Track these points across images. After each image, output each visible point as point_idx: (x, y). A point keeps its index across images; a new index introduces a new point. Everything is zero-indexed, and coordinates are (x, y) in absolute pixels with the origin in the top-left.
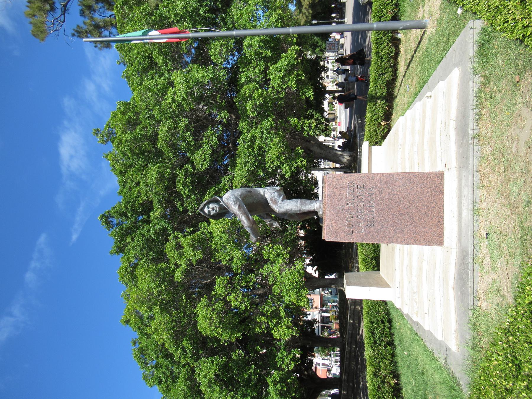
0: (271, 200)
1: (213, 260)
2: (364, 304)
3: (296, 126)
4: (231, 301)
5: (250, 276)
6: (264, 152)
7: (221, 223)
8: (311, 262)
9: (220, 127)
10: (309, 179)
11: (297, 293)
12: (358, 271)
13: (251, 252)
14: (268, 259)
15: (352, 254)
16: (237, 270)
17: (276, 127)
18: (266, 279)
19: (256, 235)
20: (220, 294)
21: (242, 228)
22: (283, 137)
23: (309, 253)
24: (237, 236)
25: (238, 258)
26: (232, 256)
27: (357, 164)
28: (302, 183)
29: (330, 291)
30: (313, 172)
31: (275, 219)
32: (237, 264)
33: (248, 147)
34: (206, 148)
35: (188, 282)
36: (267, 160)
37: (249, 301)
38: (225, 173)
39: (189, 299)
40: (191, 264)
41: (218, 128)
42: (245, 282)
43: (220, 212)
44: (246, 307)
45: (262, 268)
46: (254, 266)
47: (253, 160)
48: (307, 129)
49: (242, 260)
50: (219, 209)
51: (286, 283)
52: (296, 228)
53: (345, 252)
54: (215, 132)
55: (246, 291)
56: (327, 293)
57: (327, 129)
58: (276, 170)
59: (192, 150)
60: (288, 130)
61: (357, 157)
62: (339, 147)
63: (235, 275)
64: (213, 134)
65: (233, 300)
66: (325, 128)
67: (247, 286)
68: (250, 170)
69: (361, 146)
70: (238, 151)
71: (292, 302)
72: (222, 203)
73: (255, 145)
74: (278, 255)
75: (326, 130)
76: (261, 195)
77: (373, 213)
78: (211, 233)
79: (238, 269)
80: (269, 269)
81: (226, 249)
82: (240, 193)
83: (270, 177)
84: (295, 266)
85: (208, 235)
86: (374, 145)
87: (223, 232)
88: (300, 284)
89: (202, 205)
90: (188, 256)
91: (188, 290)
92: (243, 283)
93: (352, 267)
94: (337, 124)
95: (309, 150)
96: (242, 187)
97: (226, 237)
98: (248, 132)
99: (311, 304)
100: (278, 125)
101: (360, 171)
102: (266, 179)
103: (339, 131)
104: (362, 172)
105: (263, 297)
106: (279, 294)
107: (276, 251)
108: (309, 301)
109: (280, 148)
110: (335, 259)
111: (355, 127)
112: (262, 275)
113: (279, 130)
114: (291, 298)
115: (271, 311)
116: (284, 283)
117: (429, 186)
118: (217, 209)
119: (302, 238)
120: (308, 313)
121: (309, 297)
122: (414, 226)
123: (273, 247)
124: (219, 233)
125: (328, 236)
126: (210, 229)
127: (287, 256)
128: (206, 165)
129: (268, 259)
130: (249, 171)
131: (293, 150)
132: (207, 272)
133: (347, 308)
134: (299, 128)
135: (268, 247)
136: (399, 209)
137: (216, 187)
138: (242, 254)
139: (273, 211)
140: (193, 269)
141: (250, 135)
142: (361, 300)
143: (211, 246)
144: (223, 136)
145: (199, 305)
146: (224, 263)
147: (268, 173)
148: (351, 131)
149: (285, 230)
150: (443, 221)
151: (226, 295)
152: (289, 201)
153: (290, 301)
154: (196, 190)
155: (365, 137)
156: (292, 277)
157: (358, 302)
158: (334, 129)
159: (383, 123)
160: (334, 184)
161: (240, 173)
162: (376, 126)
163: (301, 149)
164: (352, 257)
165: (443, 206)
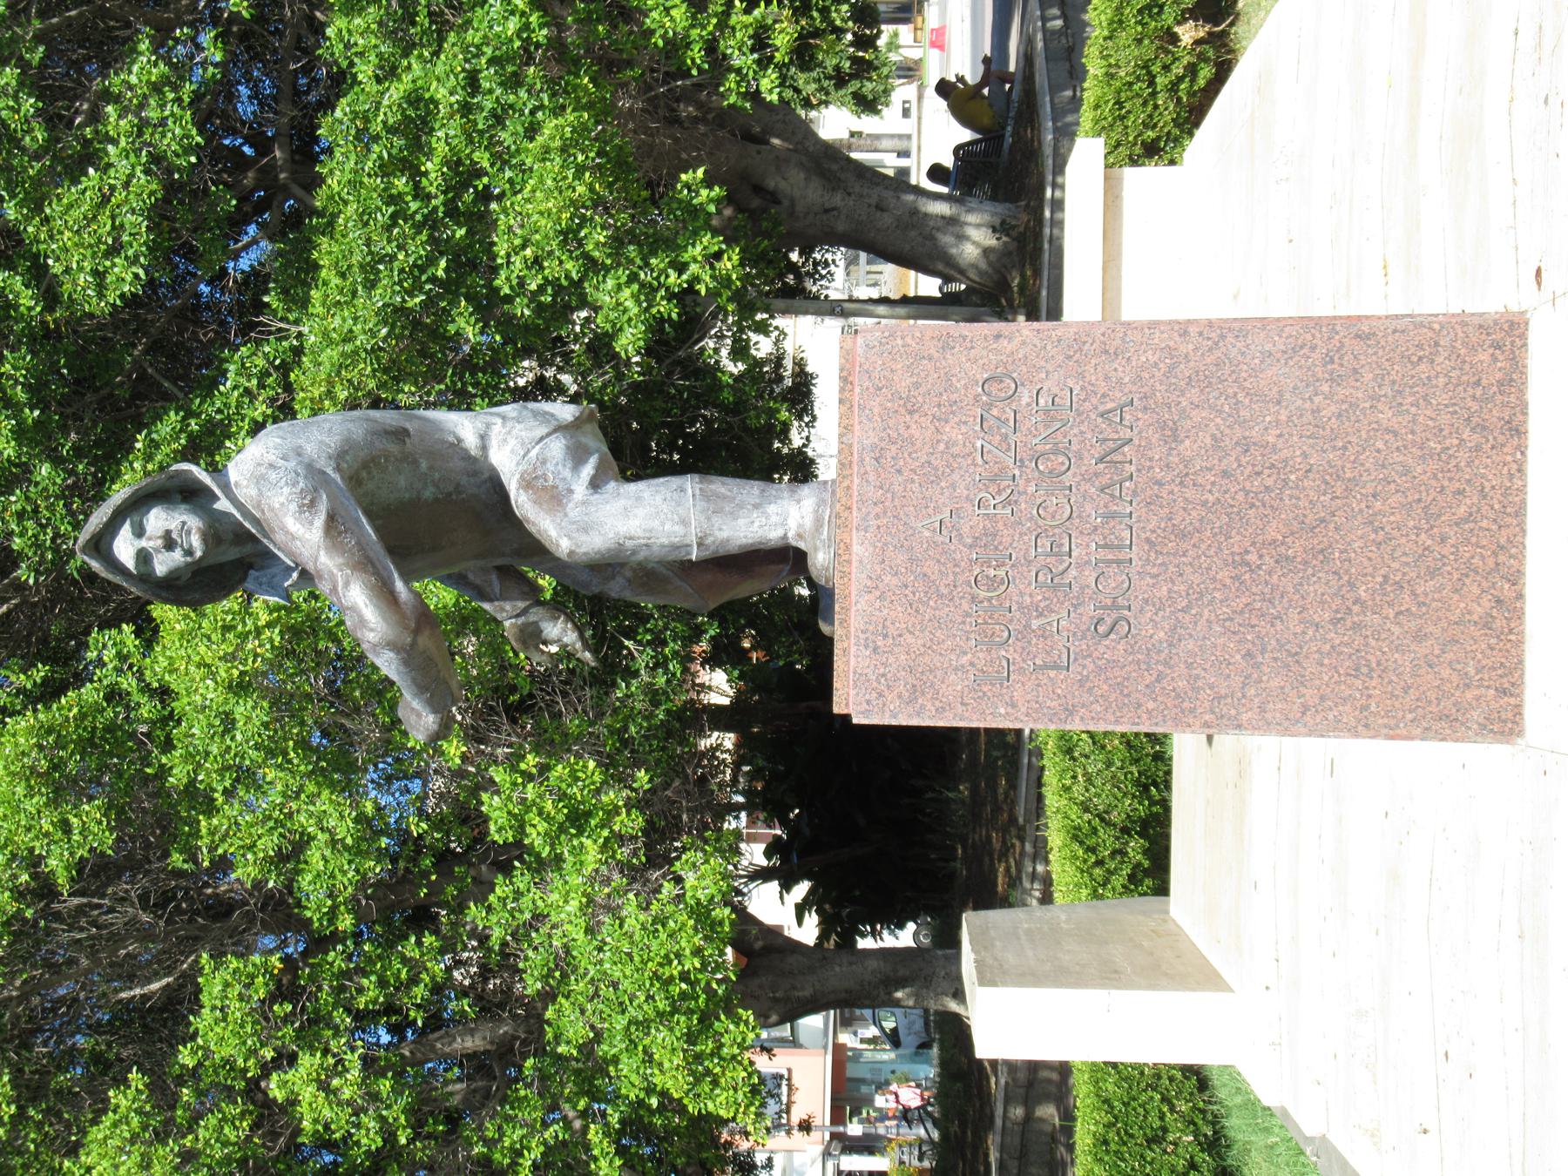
0: (527, 484)
1: (177, 859)
2: (1082, 1090)
3: (676, 46)
4: (293, 1102)
5: (410, 948)
6: (485, 196)
7: (227, 628)
8: (776, 861)
9: (206, 38)
10: (759, 363)
11: (691, 1038)
12: (1047, 899)
13: (406, 808)
14: (518, 844)
15: (1013, 804)
16: (333, 914)
17: (557, 46)
18: (506, 962)
19: (436, 691)
20: (228, 1062)
21: (356, 660)
22: (602, 111)
23: (765, 804)
24: (329, 711)
25: (333, 843)
26: (297, 830)
27: (1037, 273)
28: (718, 386)
29: (889, 1025)
30: (779, 321)
31: (557, 606)
32: (327, 881)
33: (385, 170)
34: (122, 167)
35: (24, 997)
36: (501, 249)
37: (403, 1101)
38: (246, 329)
39: (34, 1100)
40: (44, 889)
41: (199, 48)
42: (382, 983)
43: (211, 561)
44: (389, 1134)
45: (481, 899)
46: (435, 890)
47: (418, 248)
48: (743, 60)
49: (357, 852)
50: (205, 537)
51: (626, 985)
52: (686, 659)
53: (974, 790)
54: (181, 71)
55: (385, 1038)
56: (873, 1041)
57: (863, 68)
58: (561, 312)
59: (37, 182)
60: (629, 64)
61: (1038, 235)
62: (936, 173)
63: (321, 943)
64: (165, 81)
65: (308, 1093)
66: (855, 60)
67: (390, 1009)
68: (400, 310)
69: (1059, 169)
70: (322, 192)
71: (664, 1094)
72: (223, 505)
73: (429, 155)
74: (578, 819)
75: (854, 76)
76: (466, 456)
77: (1124, 554)
78: (164, 693)
79: (333, 910)
80: (526, 902)
81: (259, 788)
82: (333, 442)
83: (526, 352)
84: (678, 880)
85: (147, 709)
86: (1134, 162)
87: (240, 688)
88: (708, 990)
89: (100, 517)
90: (23, 839)
91: (27, 1046)
92: (369, 993)
93: (1014, 882)
94: (926, 37)
95: (758, 189)
96: (352, 405)
97: (259, 716)
98: (388, 72)
99: (772, 1107)
100: (570, 37)
101: (1055, 313)
102: (496, 364)
103: (932, 80)
104: (1067, 315)
105: (491, 1073)
106: (587, 1049)
107: (563, 796)
108: (764, 1089)
109: (579, 174)
110: (908, 829)
111: (1027, 58)
112: (483, 939)
113: (576, 62)
114: (656, 1067)
115: (536, 1153)
116: (615, 985)
117: (1444, 398)
118: (196, 542)
119: (720, 718)
120: (760, 1158)
121: (764, 1064)
122: (1356, 627)
123: (544, 769)
124: (211, 692)
125: (866, 693)
126: (157, 667)
127: (631, 822)
128: (125, 277)
129: (518, 844)
130: (395, 314)
131: (658, 189)
132: (146, 935)
133: (986, 1122)
134: (696, 53)
135: (514, 769)
136: (1272, 533)
137: (190, 414)
138: (361, 819)
139: (536, 550)
140: (57, 916)
141: (396, 92)
142: (1064, 1069)
143: (164, 771)
144: (231, 97)
145: (96, 1133)
146: (245, 872)
147: (508, 324)
148: (1006, 77)
149: (613, 668)
150: (1520, 596)
151: (266, 1069)
152: (633, 488)
153: (650, 1091)
154: (65, 430)
155: (1086, 116)
156: (659, 945)
157: (1044, 1082)
158: (909, 71)
159: (1188, 33)
160: (903, 382)
161: (338, 321)
162: (1148, 49)
163: (708, 182)
164: (1013, 820)
165: (1520, 512)
